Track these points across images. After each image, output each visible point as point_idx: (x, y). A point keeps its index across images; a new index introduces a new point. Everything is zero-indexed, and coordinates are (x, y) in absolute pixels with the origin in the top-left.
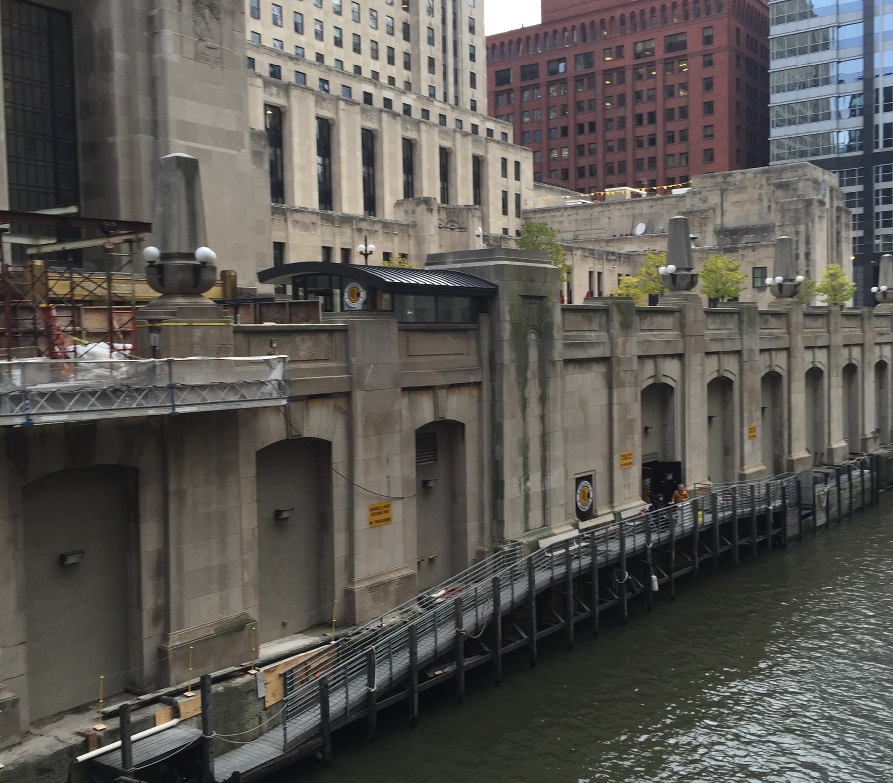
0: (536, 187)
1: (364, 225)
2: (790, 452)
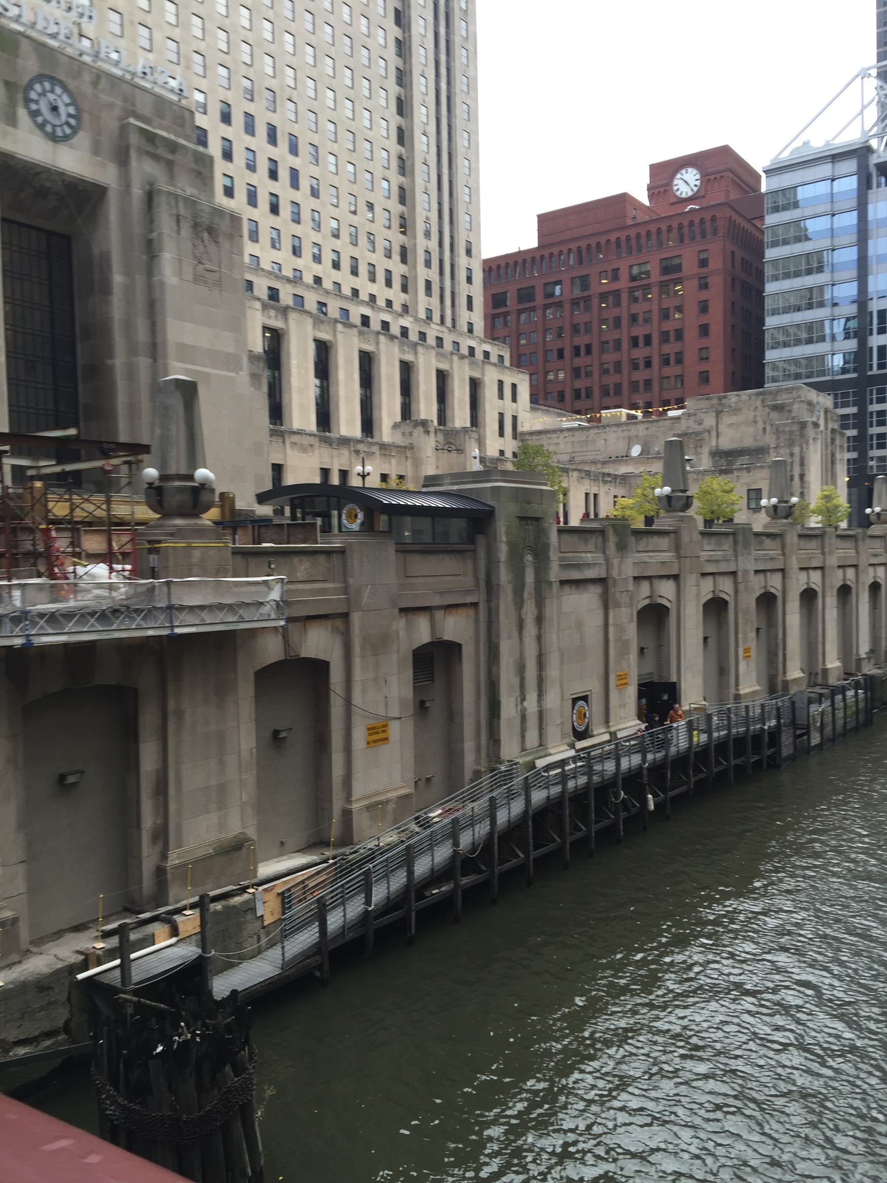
0: (532, 408)
1: (361, 447)
2: (785, 672)
